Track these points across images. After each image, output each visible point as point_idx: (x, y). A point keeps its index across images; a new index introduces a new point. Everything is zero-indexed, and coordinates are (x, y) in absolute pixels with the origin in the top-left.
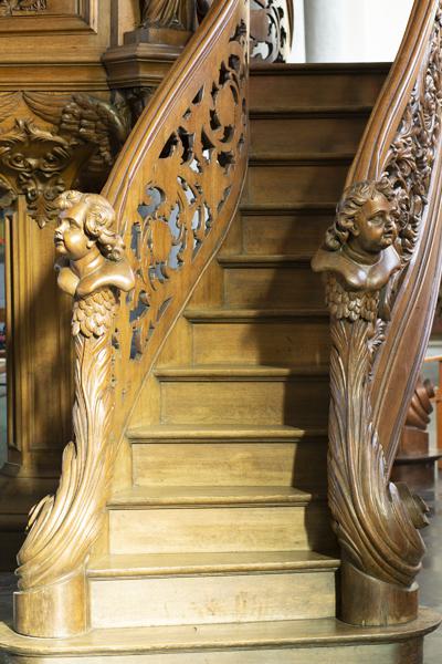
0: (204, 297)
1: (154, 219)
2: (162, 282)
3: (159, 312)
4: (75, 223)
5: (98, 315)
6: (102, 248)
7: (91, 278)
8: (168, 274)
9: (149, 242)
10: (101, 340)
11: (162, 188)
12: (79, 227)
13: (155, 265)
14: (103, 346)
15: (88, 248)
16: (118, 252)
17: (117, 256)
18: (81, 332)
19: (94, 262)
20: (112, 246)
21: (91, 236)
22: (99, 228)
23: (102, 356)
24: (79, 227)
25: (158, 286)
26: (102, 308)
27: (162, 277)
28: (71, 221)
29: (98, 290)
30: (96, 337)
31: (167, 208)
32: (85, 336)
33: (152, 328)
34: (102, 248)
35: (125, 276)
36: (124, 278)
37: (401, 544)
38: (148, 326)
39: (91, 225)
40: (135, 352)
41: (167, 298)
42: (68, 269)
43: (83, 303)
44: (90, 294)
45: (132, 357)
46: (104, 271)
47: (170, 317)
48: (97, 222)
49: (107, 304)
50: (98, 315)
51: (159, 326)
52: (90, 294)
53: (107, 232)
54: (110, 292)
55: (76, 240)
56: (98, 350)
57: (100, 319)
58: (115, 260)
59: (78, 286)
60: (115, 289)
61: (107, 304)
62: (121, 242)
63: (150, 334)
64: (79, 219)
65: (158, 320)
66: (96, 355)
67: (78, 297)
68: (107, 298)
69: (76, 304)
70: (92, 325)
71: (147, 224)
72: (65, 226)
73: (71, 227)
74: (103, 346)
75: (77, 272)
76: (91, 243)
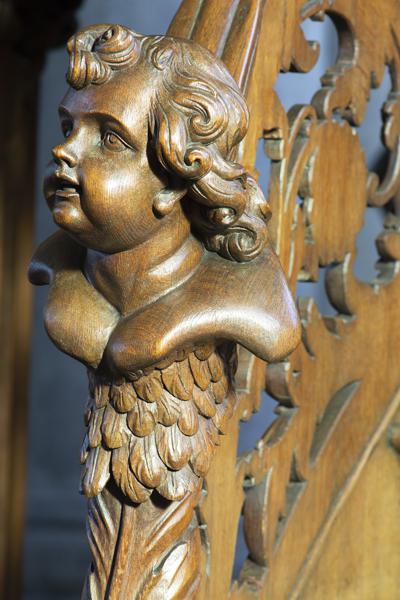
0: (227, 393)
1: (320, 116)
2: (331, 326)
3: (321, 427)
4: (121, 132)
5: (173, 435)
6: (201, 216)
7: (161, 314)
8: (353, 298)
9: (302, 194)
10: (175, 516)
11: (347, 13)
12: (131, 144)
13: (315, 268)
14: (177, 536)
15: (158, 214)
16: (249, 231)
17: (244, 244)
18: (113, 486)
19: (169, 263)
20: (235, 212)
21: (165, 171)
22: (202, 154)
23: (175, 564)
24: (131, 144)
25: (321, 340)
26: (186, 411)
27: (332, 313)
28: (108, 128)
29: (179, 351)
30: (161, 501)
31: (358, 83)
32: (126, 500)
33: (296, 478)
34: (201, 216)
35: (268, 309)
36: (262, 318)
37: (386, 58)
38: (287, 473)
39: (175, 139)
40: (251, 555)
41: (341, 383)
42: (74, 277)
43: (127, 393)
44: (154, 364)
45: (236, 575)
46: (199, 291)
47: (350, 449)
48: (193, 133)
49: (203, 398)
50: (173, 435)
51: (317, 473)
52: (154, 364)
53: (221, 164)
54: (213, 358)
55: (122, 184)
56: (160, 547)
57: (177, 444)
58: (231, 255)
59: (115, 336)
60: (226, 346)
61: (203, 398)
62: (258, 200)
63: (291, 496)
64: (133, 119)
65: (313, 453)
66: (155, 563)
67: (110, 372)
68: (204, 380)
69: (102, 395)
70: (153, 465)
71: (301, 134)
72: (83, 142)
73: (106, 146)
74: (177, 536)
75: (112, 290)
76: (167, 201)
